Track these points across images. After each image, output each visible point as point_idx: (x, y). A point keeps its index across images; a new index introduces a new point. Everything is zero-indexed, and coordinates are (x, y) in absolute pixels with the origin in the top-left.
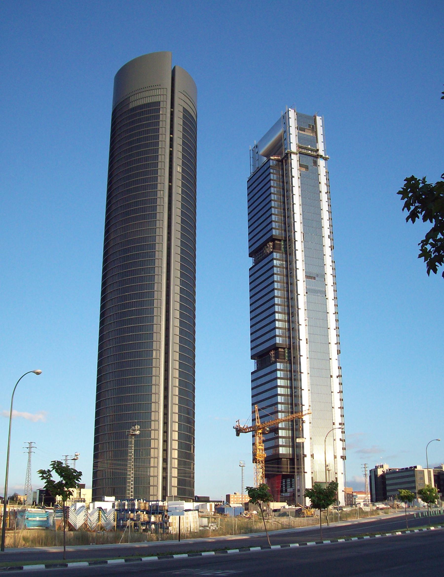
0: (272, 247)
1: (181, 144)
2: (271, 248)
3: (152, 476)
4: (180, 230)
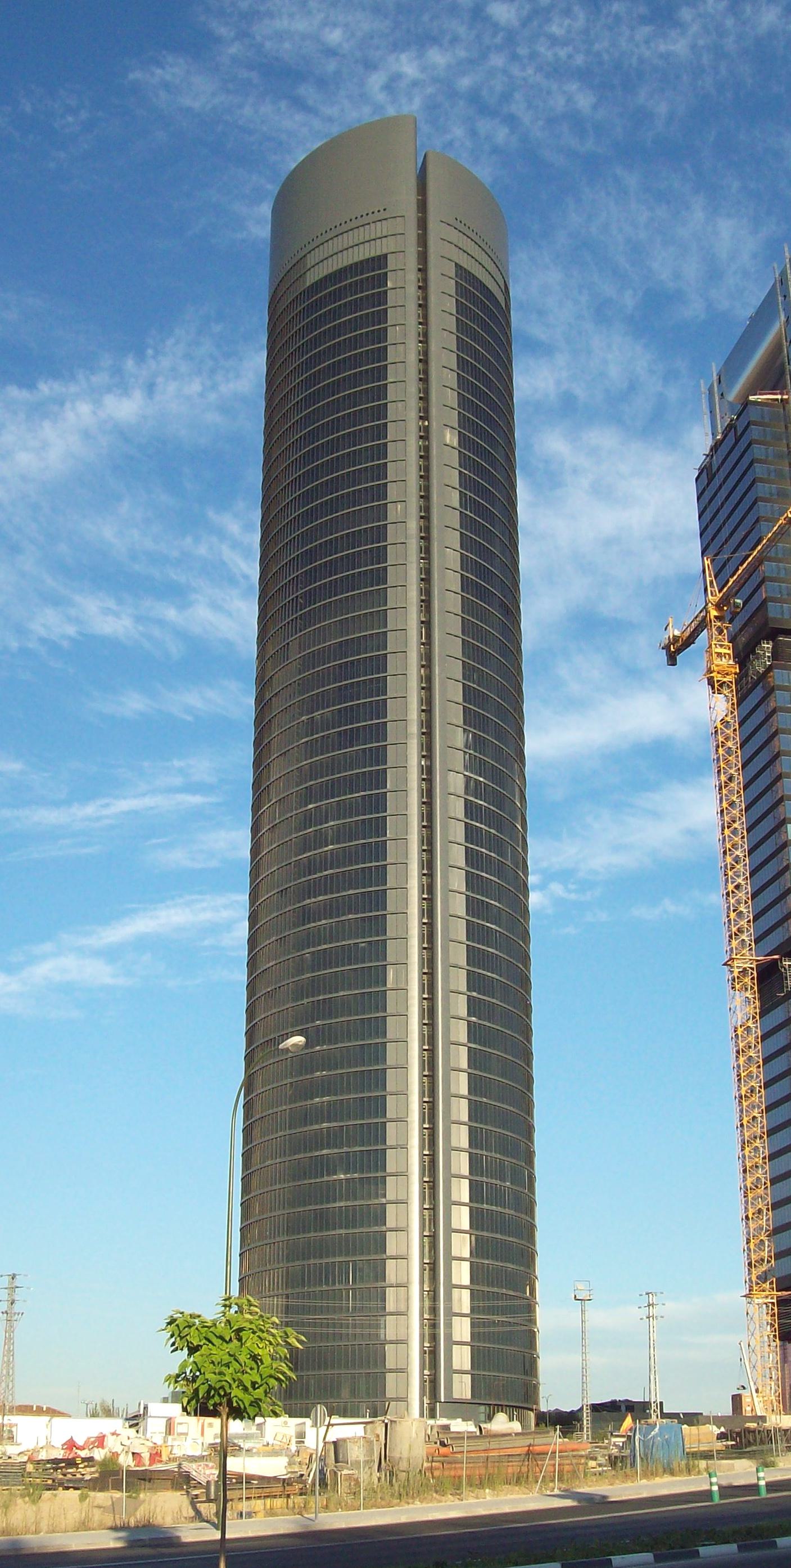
0: (770, 655)
1: (455, 367)
2: (769, 657)
3: (391, 1342)
4: (460, 655)
